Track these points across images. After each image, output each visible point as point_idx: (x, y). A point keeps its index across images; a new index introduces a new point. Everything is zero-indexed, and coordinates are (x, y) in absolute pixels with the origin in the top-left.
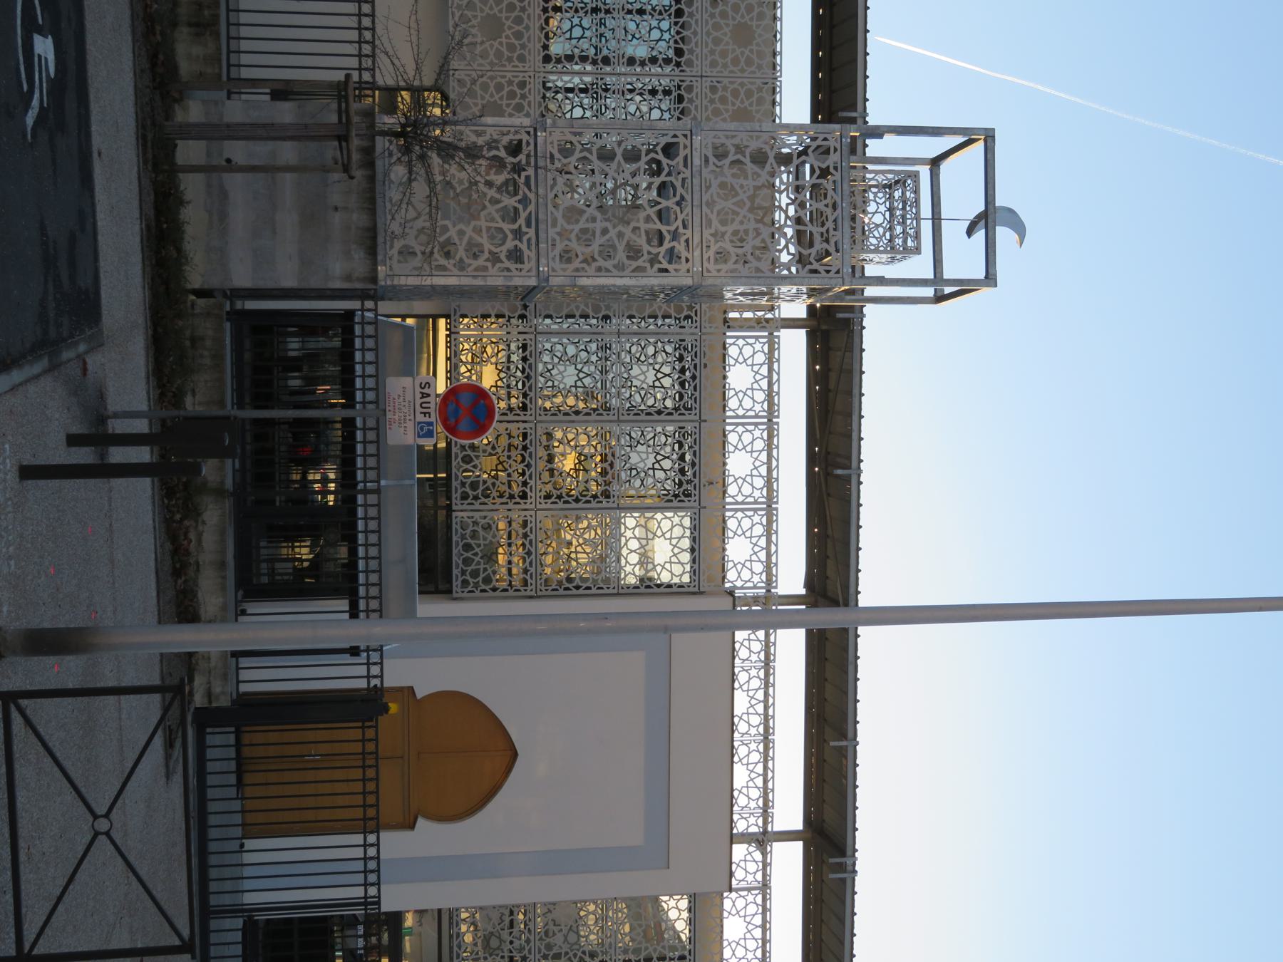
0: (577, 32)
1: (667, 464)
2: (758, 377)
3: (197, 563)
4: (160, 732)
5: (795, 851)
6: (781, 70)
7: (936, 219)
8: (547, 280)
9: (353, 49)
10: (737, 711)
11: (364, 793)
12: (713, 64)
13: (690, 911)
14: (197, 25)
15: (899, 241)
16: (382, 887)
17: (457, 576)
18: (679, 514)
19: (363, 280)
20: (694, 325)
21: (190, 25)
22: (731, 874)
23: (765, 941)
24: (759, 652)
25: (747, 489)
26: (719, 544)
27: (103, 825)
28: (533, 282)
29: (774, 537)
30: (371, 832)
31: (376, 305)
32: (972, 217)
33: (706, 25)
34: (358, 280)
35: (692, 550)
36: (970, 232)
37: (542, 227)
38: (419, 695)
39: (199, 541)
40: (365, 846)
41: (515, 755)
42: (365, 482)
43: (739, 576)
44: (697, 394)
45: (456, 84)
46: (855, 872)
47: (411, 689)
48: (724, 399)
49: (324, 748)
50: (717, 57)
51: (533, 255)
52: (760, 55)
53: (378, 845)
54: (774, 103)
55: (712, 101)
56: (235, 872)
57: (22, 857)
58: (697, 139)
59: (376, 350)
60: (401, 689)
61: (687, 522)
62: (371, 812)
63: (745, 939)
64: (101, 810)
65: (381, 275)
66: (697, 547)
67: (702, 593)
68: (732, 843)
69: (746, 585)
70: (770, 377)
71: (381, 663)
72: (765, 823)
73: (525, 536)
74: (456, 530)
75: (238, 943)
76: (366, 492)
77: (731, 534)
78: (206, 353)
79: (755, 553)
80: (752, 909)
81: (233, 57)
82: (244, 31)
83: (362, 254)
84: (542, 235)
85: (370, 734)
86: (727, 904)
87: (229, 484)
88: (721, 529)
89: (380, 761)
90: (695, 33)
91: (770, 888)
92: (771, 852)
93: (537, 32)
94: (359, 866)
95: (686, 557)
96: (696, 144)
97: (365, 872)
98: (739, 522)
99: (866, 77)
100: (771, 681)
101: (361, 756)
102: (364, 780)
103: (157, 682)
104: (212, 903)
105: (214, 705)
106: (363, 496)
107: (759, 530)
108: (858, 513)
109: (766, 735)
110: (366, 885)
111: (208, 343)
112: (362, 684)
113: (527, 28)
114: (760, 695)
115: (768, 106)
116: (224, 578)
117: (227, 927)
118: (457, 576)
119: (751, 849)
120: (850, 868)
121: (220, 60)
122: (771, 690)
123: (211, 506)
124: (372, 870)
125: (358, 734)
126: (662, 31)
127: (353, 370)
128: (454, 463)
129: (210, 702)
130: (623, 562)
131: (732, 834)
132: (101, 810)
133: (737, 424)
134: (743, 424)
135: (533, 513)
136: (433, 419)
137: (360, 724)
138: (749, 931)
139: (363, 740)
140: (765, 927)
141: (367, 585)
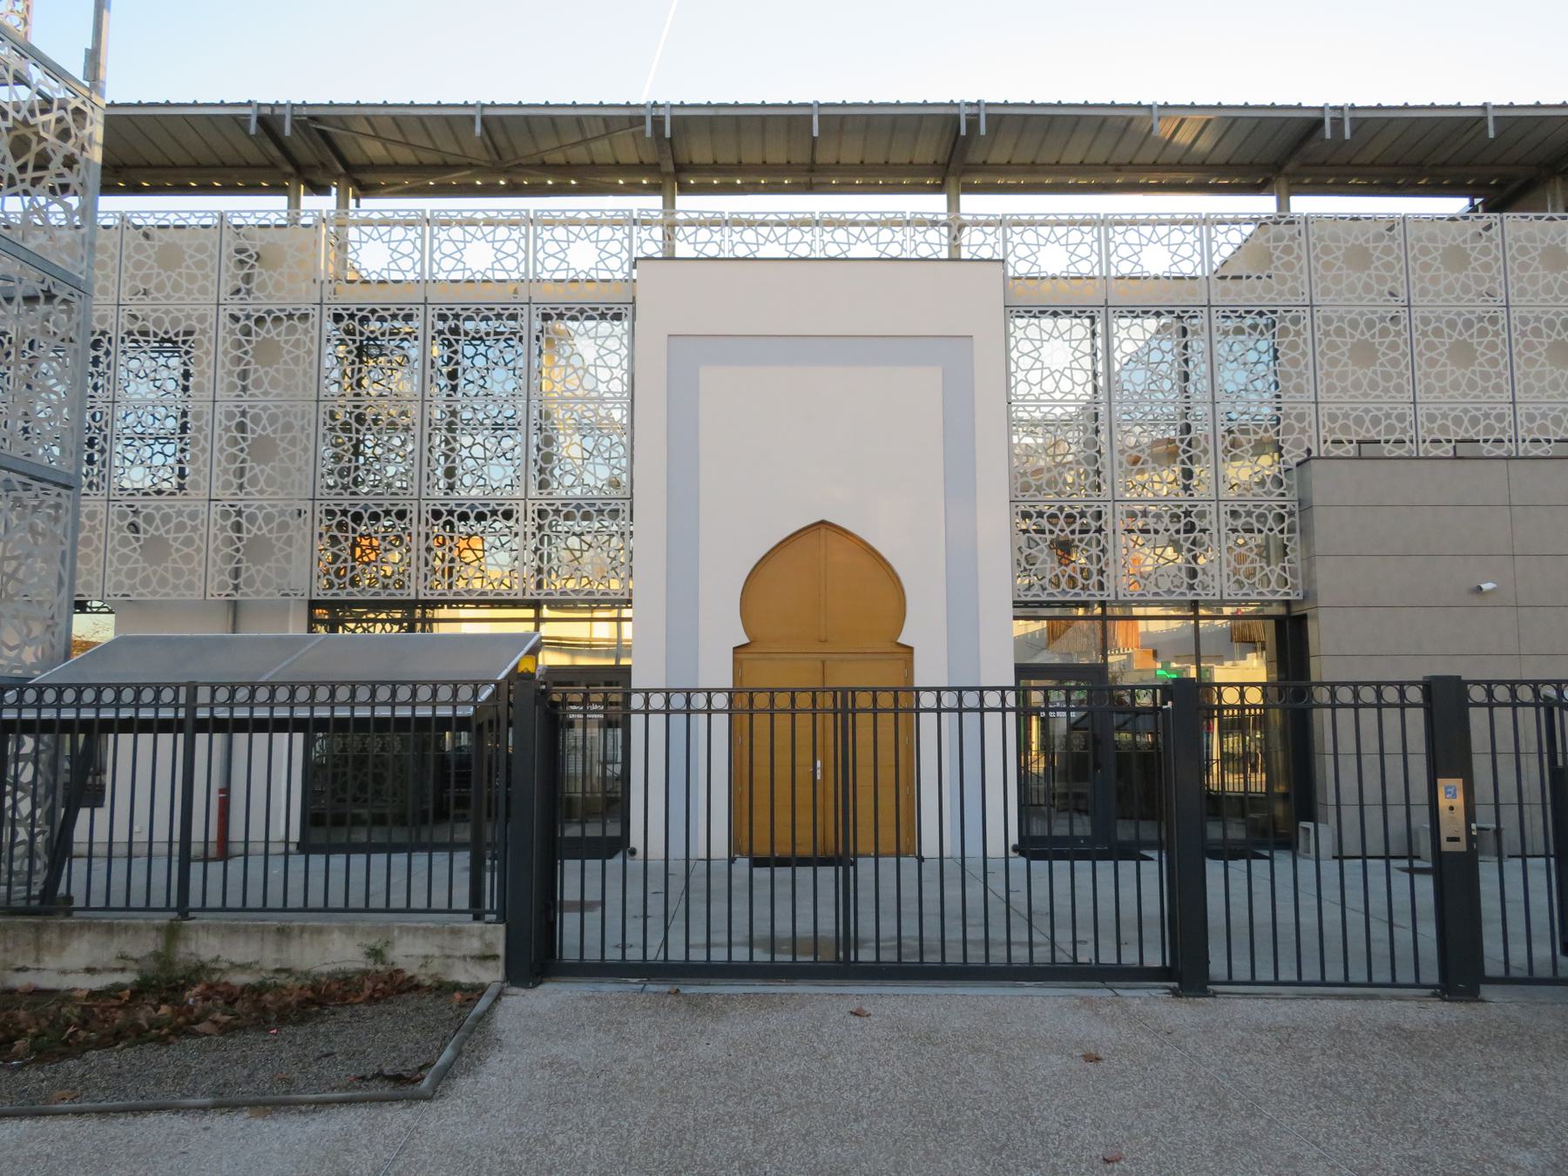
0: (158, 460)
1: (1026, 346)
2: (772, 237)
6: (1193, 214)
9: (971, 719)
16: (983, 684)
17: (389, 595)
18: (1115, 330)
20: (1199, 314)
24: (985, 233)
25: (1084, 251)
26: (1047, 285)
30: (730, 701)
31: (637, 691)
33: (177, 310)
35: (1055, 314)
38: (744, 640)
40: (1334, 707)
41: (823, 522)
43: (1123, 259)
45: (1030, 593)
46: (1484, 107)
47: (736, 649)
48: (1182, 278)
49: (804, 756)
50: (1286, 288)
53: (1355, 684)
56: (677, 867)
61: (1124, 322)
62: (885, 700)
63: (1169, 245)
66: (1051, 310)
69: (523, 246)
72: (934, 223)
74: (334, 595)
75: (604, 865)
77: (1138, 269)
79: (568, 241)
88: (1131, 281)
89: (828, 685)
91: (1004, 215)
92: (1157, 214)
95: (1064, 323)
97: (1380, 705)
98: (1086, 259)
100: (1027, 218)
101: (901, 716)
102: (1356, 707)
106: (199, 709)
107: (1030, 236)
109: (1208, 222)
114: (1146, 230)
118: (389, 595)
119: (681, 236)
120: (974, 110)
126: (476, 355)
130: (594, 394)
131: (950, 260)
134: (432, 252)
135: (529, 503)
138: (1047, 240)
139: (982, 710)
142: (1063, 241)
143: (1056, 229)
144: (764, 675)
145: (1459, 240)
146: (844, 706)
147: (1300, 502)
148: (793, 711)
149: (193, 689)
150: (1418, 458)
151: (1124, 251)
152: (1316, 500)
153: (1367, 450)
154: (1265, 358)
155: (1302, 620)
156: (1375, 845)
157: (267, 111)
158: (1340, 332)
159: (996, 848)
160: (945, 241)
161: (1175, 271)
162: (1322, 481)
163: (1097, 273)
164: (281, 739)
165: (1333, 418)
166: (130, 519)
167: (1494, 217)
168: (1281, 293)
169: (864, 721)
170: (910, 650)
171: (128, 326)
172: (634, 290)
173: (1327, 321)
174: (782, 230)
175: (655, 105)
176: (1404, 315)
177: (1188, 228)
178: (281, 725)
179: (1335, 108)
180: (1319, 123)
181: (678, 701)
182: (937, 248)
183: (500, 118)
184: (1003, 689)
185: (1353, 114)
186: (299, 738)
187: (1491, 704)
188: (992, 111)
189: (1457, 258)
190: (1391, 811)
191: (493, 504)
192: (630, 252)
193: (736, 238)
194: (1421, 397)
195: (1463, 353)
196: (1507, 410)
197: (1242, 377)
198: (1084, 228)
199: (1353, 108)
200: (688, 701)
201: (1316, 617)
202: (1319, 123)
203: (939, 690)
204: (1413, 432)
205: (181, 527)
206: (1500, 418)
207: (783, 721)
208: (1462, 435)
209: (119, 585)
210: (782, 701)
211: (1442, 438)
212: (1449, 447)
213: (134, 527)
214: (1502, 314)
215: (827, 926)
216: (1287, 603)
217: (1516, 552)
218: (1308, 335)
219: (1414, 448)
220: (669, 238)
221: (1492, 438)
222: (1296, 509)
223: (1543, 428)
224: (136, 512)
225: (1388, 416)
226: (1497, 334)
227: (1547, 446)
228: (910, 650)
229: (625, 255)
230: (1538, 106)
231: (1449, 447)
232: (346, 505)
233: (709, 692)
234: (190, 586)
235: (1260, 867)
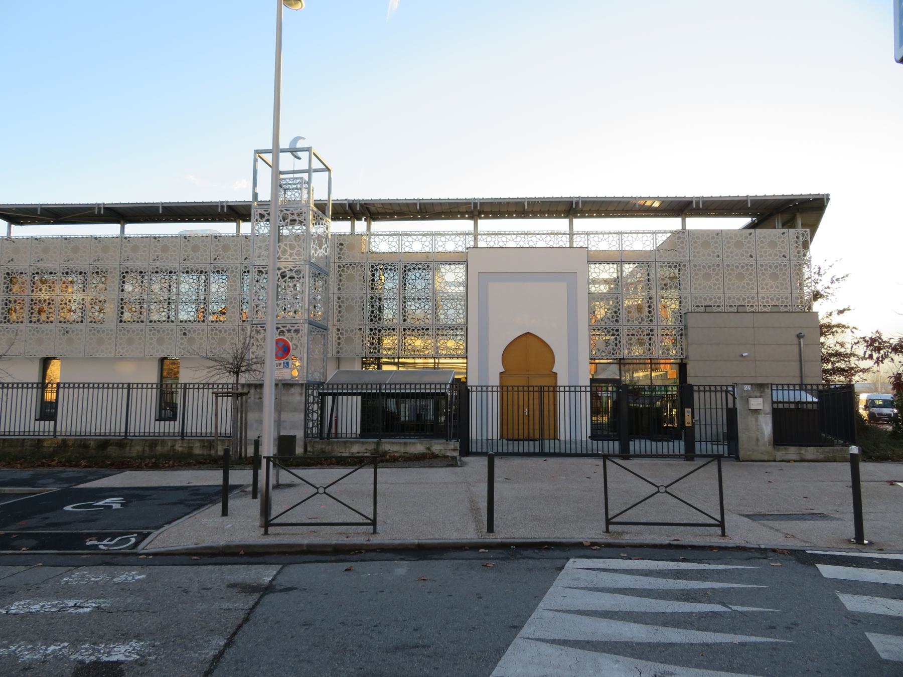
3: (404, 453)
4: (291, 470)
5: (481, 222)
7: (294, 172)
8: (306, 320)
10: (545, 245)
11: (565, 391)
12: (236, 259)
13: (630, 263)
14: (210, 447)
15: (299, 186)
19: (302, 388)
21: (210, 450)
22: (581, 247)
23: (610, 233)
27: (321, 490)
28: (306, 325)
29: (446, 233)
32: (293, 157)
34: (302, 390)
35: (450, 264)
36: (299, 158)
37: (287, 322)
39: (396, 452)
40: (549, 391)
41: (528, 333)
42: (377, 389)
44: (390, 263)
46: (747, 196)
47: (500, 373)
51: (296, 325)
52: (233, 241)
53: (704, 386)
54: (344, 235)
55: (732, 257)
56: (484, 442)
57: (313, 521)
58: (256, 264)
59: (395, 384)
60: (501, 377)
64: (315, 491)
65: (303, 382)
67: (467, 260)
68: (477, 248)
70: (450, 235)
71: (581, 386)
73: (443, 329)
76: (380, 389)
78: (327, 448)
80: (596, 239)
81: (161, 435)
82: (204, 431)
83: (292, 389)
84: (290, 322)
85: (474, 389)
86: (594, 249)
87: (376, 440)
90: (225, 266)
93: (193, 324)
94: (573, 394)
95: (453, 267)
96: (258, 264)
99: (440, 199)
103: (373, 470)
104: (538, 451)
105: (458, 448)
107: (443, 238)
108: (538, 198)
110: (487, 391)
111: (323, 446)
112: (154, 391)
113: (192, 328)
115: (173, 239)
116: (410, 443)
117: (596, 446)
120: (578, 199)
121: (223, 440)
122: (507, 233)
123: (383, 447)
124: (574, 389)
125: (562, 394)
127: (403, 393)
128: (67, 356)
129: (457, 450)
132: (315, 491)
133: (435, 247)
134: (402, 245)
136: (282, 362)
137: (470, 393)
139: (492, 391)
140: (603, 233)
141: (410, 389)
142: (485, 240)
143: (605, 235)
144: (511, 382)
145: (707, 239)
146: (541, 390)
147: (685, 326)
148: (513, 391)
149: (380, 385)
150: (758, 312)
151: (627, 243)
152: (689, 326)
153: (708, 309)
154: (195, 281)
155: (685, 365)
156: (704, 438)
157: (351, 202)
158: (699, 270)
159: (584, 438)
160: (568, 240)
161: (423, 250)
162: (692, 320)
163: (431, 251)
164: (355, 398)
165: (763, 298)
166: (184, 331)
167: (785, 230)
168: (679, 257)
169: (546, 394)
170: (556, 374)
171: (244, 270)
172: (467, 256)
173: (695, 266)
174: (387, 237)
175: (474, 199)
176: (788, 263)
177: (583, 236)
178: (354, 394)
179: (697, 197)
180: (692, 202)
181: (484, 389)
182: (565, 243)
183: (424, 203)
184: (497, 386)
185: (703, 199)
186: (359, 398)
187: (699, 391)
188: (583, 200)
189: (739, 244)
190: (702, 426)
191: (389, 326)
192: (465, 245)
193: (559, 239)
194: (760, 291)
195: (774, 276)
196: (789, 296)
197: (187, 286)
198: (521, 236)
199: (703, 197)
200: (487, 389)
201: (688, 364)
202: (692, 202)
203: (523, 386)
204: (723, 303)
205: (168, 334)
206: (753, 298)
207: (515, 393)
208: (740, 304)
209: (180, 352)
210: (510, 389)
211: (700, 305)
212: (735, 308)
213: (185, 334)
214: (788, 263)
215: (123, 430)
216: (682, 359)
217: (756, 343)
218: (688, 271)
219: (791, 308)
220: (476, 240)
221: (750, 305)
222: (683, 328)
223: (767, 302)
224: (185, 330)
225: (782, 298)
226: (719, 270)
227: (769, 308)
228: (556, 374)
229: (464, 246)
230: (774, 196)
231: (735, 308)
232: (376, 326)
233: (534, 386)
234: (110, 352)
235: (671, 443)
